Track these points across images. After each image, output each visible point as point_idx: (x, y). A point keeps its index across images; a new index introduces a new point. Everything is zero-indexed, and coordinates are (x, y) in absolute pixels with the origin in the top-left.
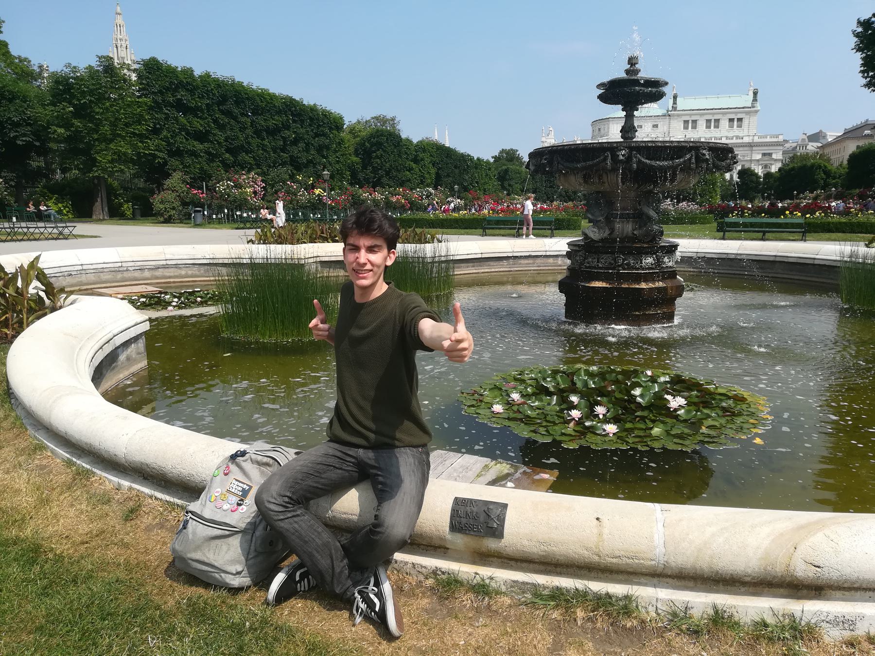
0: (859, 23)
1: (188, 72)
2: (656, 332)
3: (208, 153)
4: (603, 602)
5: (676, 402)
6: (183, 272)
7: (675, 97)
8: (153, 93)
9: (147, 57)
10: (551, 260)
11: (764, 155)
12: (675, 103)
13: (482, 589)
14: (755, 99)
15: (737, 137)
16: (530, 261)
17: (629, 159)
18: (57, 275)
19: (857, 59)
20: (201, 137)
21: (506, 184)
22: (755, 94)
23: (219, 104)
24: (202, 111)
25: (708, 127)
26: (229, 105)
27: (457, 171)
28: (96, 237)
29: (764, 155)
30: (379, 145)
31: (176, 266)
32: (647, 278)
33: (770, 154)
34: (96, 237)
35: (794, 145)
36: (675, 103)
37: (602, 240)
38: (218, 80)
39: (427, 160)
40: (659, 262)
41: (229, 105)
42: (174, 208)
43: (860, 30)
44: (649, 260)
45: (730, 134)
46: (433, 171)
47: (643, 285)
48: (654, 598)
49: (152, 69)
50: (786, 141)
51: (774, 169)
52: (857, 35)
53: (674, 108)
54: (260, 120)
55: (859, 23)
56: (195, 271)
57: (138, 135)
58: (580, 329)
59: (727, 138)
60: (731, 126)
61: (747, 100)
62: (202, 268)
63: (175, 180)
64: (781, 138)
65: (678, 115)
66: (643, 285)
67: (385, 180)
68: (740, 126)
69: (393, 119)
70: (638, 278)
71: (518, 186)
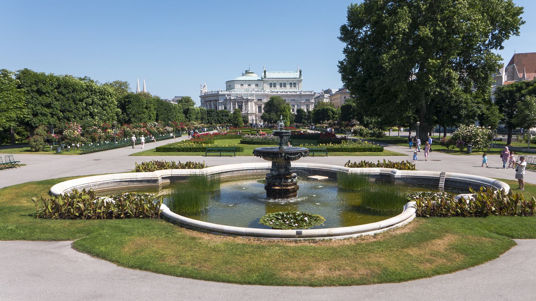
0: (339, 62)
1: (43, 75)
2: (292, 200)
3: (51, 114)
4: (312, 240)
5: (306, 219)
6: (110, 185)
7: (265, 72)
8: (27, 86)
9: (22, 69)
10: (245, 171)
11: (306, 100)
12: (265, 74)
13: (300, 240)
14: (300, 75)
15: (294, 92)
16: (238, 172)
17: (285, 155)
18: (495, 235)
19: (340, 76)
20: (48, 106)
21: (188, 115)
22: (300, 72)
23: (56, 88)
24: (49, 93)
25: (281, 86)
26: (62, 89)
27: (165, 111)
28: (25, 165)
29: (306, 100)
30: (129, 102)
31: (107, 183)
32: (290, 186)
33: (309, 100)
34: (25, 165)
35: (319, 95)
36: (265, 74)
37: (277, 175)
38: (58, 79)
39: (152, 108)
40: (292, 181)
41: (62, 89)
42: (41, 144)
43: (340, 65)
44: (290, 180)
45: (291, 90)
46: (155, 113)
47: (289, 188)
48: (317, 238)
49: (25, 73)
50: (315, 93)
51: (311, 109)
52: (339, 67)
53: (265, 77)
54: (74, 95)
55: (339, 62)
56: (114, 184)
57: (19, 108)
58: (271, 201)
59: (290, 92)
60: (291, 87)
61: (297, 75)
62: (117, 183)
63: (41, 130)
64: (313, 93)
65: (267, 81)
66: (289, 188)
67: (133, 119)
68: (295, 87)
69: (126, 82)
70: (287, 186)
71: (194, 117)
